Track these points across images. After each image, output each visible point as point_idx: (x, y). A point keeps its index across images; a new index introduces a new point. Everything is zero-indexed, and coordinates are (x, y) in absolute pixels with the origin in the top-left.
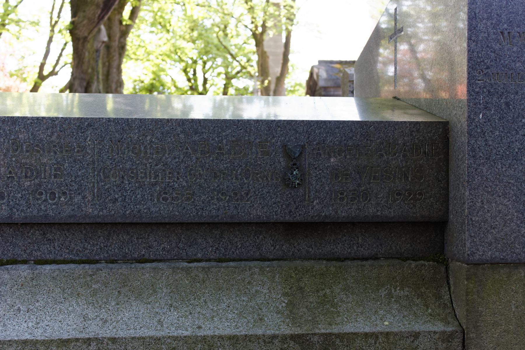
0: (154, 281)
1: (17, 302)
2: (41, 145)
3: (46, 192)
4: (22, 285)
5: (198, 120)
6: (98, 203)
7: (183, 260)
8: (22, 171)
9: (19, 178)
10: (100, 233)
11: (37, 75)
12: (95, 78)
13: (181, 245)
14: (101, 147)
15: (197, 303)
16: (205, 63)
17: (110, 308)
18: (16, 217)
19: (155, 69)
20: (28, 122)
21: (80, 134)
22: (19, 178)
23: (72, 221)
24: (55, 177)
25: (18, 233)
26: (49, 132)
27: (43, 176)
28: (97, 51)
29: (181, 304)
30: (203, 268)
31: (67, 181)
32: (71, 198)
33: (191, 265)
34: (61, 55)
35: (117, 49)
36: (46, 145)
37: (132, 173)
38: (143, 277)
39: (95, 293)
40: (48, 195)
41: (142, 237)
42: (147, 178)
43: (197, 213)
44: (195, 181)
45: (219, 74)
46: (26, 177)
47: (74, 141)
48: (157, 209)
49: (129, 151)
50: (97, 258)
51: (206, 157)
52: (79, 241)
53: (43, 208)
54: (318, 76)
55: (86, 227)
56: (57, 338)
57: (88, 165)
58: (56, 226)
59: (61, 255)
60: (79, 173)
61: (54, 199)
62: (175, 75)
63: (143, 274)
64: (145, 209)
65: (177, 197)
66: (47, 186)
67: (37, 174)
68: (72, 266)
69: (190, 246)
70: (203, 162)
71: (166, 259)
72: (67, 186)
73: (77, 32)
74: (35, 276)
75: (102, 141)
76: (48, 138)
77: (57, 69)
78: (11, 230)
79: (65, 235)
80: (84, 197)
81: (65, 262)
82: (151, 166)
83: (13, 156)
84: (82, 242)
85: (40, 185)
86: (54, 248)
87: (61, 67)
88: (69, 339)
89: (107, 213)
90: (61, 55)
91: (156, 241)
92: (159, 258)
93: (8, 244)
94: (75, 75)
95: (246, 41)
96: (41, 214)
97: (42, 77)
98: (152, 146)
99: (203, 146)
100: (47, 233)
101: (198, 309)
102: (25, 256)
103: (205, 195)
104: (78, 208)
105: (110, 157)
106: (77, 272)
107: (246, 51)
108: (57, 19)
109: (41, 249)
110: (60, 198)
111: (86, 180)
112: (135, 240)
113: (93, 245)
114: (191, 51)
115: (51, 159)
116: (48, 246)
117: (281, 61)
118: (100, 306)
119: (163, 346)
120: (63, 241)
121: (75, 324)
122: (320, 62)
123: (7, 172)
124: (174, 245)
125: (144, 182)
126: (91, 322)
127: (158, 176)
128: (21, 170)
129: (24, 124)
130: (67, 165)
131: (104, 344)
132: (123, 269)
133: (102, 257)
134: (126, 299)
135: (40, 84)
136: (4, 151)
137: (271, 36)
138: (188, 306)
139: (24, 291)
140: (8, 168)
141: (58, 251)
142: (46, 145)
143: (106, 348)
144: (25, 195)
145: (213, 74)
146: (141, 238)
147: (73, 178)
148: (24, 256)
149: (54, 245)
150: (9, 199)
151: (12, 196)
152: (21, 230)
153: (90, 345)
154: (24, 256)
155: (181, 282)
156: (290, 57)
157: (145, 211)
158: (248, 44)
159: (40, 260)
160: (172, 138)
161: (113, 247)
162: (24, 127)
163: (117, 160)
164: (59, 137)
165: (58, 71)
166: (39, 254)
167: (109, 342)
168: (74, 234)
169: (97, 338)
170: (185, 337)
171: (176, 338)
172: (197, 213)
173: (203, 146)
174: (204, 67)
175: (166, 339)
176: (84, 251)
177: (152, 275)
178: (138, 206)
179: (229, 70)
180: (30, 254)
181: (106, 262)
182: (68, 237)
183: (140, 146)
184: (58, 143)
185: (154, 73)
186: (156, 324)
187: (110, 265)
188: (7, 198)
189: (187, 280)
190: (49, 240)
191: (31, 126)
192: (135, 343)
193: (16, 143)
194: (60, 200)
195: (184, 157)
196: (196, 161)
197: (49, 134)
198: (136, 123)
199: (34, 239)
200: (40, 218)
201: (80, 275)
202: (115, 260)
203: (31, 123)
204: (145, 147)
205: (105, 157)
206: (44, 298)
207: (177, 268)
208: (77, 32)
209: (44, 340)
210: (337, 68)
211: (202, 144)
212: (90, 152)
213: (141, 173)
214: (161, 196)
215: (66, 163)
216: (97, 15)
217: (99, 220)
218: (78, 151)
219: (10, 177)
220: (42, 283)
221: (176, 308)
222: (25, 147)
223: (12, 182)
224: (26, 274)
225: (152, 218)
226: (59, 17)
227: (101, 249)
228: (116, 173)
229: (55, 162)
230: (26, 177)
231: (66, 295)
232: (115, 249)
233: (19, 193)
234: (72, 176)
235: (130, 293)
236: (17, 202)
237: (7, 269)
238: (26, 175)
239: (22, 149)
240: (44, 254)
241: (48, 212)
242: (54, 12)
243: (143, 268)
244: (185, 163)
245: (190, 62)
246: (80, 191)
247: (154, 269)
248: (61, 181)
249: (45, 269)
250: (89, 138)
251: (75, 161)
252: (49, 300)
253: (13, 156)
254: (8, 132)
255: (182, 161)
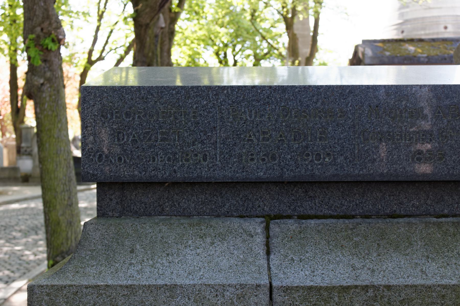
0: (408, 234)
1: (289, 252)
2: (307, 111)
3: (312, 154)
4: (292, 238)
5: (449, 85)
6: (359, 163)
7: (431, 215)
8: (291, 135)
9: (289, 141)
10: (355, 191)
11: (86, 60)
12: (155, 61)
13: (429, 202)
14: (361, 112)
15: (451, 255)
16: (234, 46)
17: (373, 259)
18: (286, 176)
19: (191, 53)
20: (297, 90)
21: (342, 100)
22: (289, 141)
23: (335, 179)
24: (320, 140)
25: (283, 190)
26: (315, 99)
27: (309, 139)
28: (156, 36)
29: (437, 256)
30: (453, 223)
31: (330, 143)
32: (335, 159)
33: (440, 220)
34: (107, 42)
35: (167, 35)
36: (312, 111)
37: (389, 135)
38: (398, 231)
39: (356, 245)
40: (314, 156)
41: (393, 194)
42: (402, 140)
43: (448, 172)
44: (447, 142)
45: (249, 56)
46: (295, 140)
47: (337, 107)
48: (412, 169)
49: (386, 115)
50: (353, 213)
51: (457, 120)
52: (337, 198)
53: (310, 168)
54: (363, 54)
55: (344, 186)
56: (338, 285)
57: (349, 128)
58: (317, 185)
59: (321, 211)
60: (342, 136)
61: (320, 160)
62: (208, 58)
63: (398, 228)
64: (401, 168)
65: (430, 157)
66: (313, 148)
67: (304, 137)
68: (334, 221)
69: (437, 203)
70: (454, 124)
71: (415, 214)
72: (331, 148)
73: (140, 19)
74: (303, 229)
75: (362, 106)
76: (314, 104)
77: (104, 55)
78: (277, 188)
79: (325, 192)
80: (346, 158)
81: (325, 217)
82: (406, 128)
83: (283, 122)
84: (339, 199)
85: (307, 147)
86: (315, 204)
87: (107, 53)
88: (349, 286)
89: (366, 172)
90: (107, 42)
91: (406, 198)
92: (409, 213)
93: (275, 201)
94: (137, 59)
95: (273, 25)
96: (308, 173)
97: (90, 63)
98: (406, 110)
99: (454, 109)
100: (309, 191)
101: (454, 261)
102: (289, 212)
103: (456, 155)
104: (341, 167)
105: (369, 121)
106: (340, 226)
107: (273, 34)
108: (103, 10)
109: (303, 206)
110: (324, 158)
111: (347, 143)
112: (387, 197)
113: (350, 201)
114: (224, 34)
115: (317, 124)
116: (310, 202)
117: (310, 43)
118: (364, 257)
119: (433, 294)
120: (323, 198)
121: (347, 272)
122: (364, 42)
123: (278, 136)
124: (422, 201)
125: (400, 143)
126: (360, 271)
127: (412, 138)
128: (290, 133)
129: (293, 92)
130: (330, 128)
131: (380, 291)
132: (381, 224)
133: (357, 212)
134: (385, 251)
135: (89, 69)
136: (276, 117)
137: (301, 19)
138: (443, 258)
139: (294, 243)
140: (279, 132)
141: (319, 207)
142: (312, 111)
143: (382, 295)
144: (293, 156)
145: (243, 56)
146: (393, 195)
147: (336, 141)
148: (289, 212)
149: (315, 202)
150: (280, 160)
151: (283, 158)
152: (286, 188)
153: (368, 292)
154: (289, 212)
155: (434, 236)
156: (319, 38)
157: (401, 170)
158: (275, 27)
159: (302, 215)
160: (425, 102)
161: (367, 203)
162: (293, 95)
163: (375, 123)
164: (323, 103)
165: (104, 57)
166: (302, 209)
167: (385, 289)
168: (332, 191)
169: (373, 286)
170: (454, 285)
171: (445, 287)
172: (448, 172)
173: (454, 109)
174: (234, 50)
175: (436, 287)
176: (342, 207)
177: (407, 229)
178: (394, 166)
179: (258, 51)
180: (294, 210)
181: (361, 218)
182: (327, 195)
183: (396, 110)
184: (323, 109)
185: (190, 56)
186: (420, 273)
187: (367, 220)
188: (278, 159)
189: (440, 234)
190: (311, 197)
191: (299, 94)
192: (408, 291)
193: (286, 109)
194: (324, 160)
195: (436, 120)
196: (447, 124)
197: (315, 100)
198: (393, 89)
199: (298, 196)
200: (307, 177)
201: (342, 229)
202: (370, 216)
203: (299, 91)
204: (401, 112)
205: (365, 121)
206: (312, 249)
207: (429, 222)
208: (140, 19)
209: (327, 287)
210: (380, 47)
211: (452, 108)
212: (351, 116)
213: (397, 135)
214: (415, 156)
215: (329, 126)
216: (158, 4)
217: (360, 179)
218: (341, 116)
219: (280, 140)
220: (309, 236)
221: (433, 259)
222: (293, 113)
223: (282, 144)
224: (294, 228)
225: (407, 176)
226: (105, 8)
227: (356, 205)
228: (374, 136)
229: (320, 126)
230: (295, 140)
231: (331, 247)
232: (369, 206)
233: (289, 154)
234: (335, 139)
235: (388, 246)
236: (287, 163)
237: (277, 223)
238: (295, 138)
239: (291, 114)
240: (306, 210)
241: (314, 171)
242: (101, 4)
243: (398, 223)
244: (437, 126)
245: (221, 45)
246: (342, 153)
247: (408, 223)
248: (326, 143)
249: (311, 224)
250: (350, 104)
251: (337, 125)
252: (317, 251)
253: (283, 122)
254: (279, 100)
255: (435, 123)
